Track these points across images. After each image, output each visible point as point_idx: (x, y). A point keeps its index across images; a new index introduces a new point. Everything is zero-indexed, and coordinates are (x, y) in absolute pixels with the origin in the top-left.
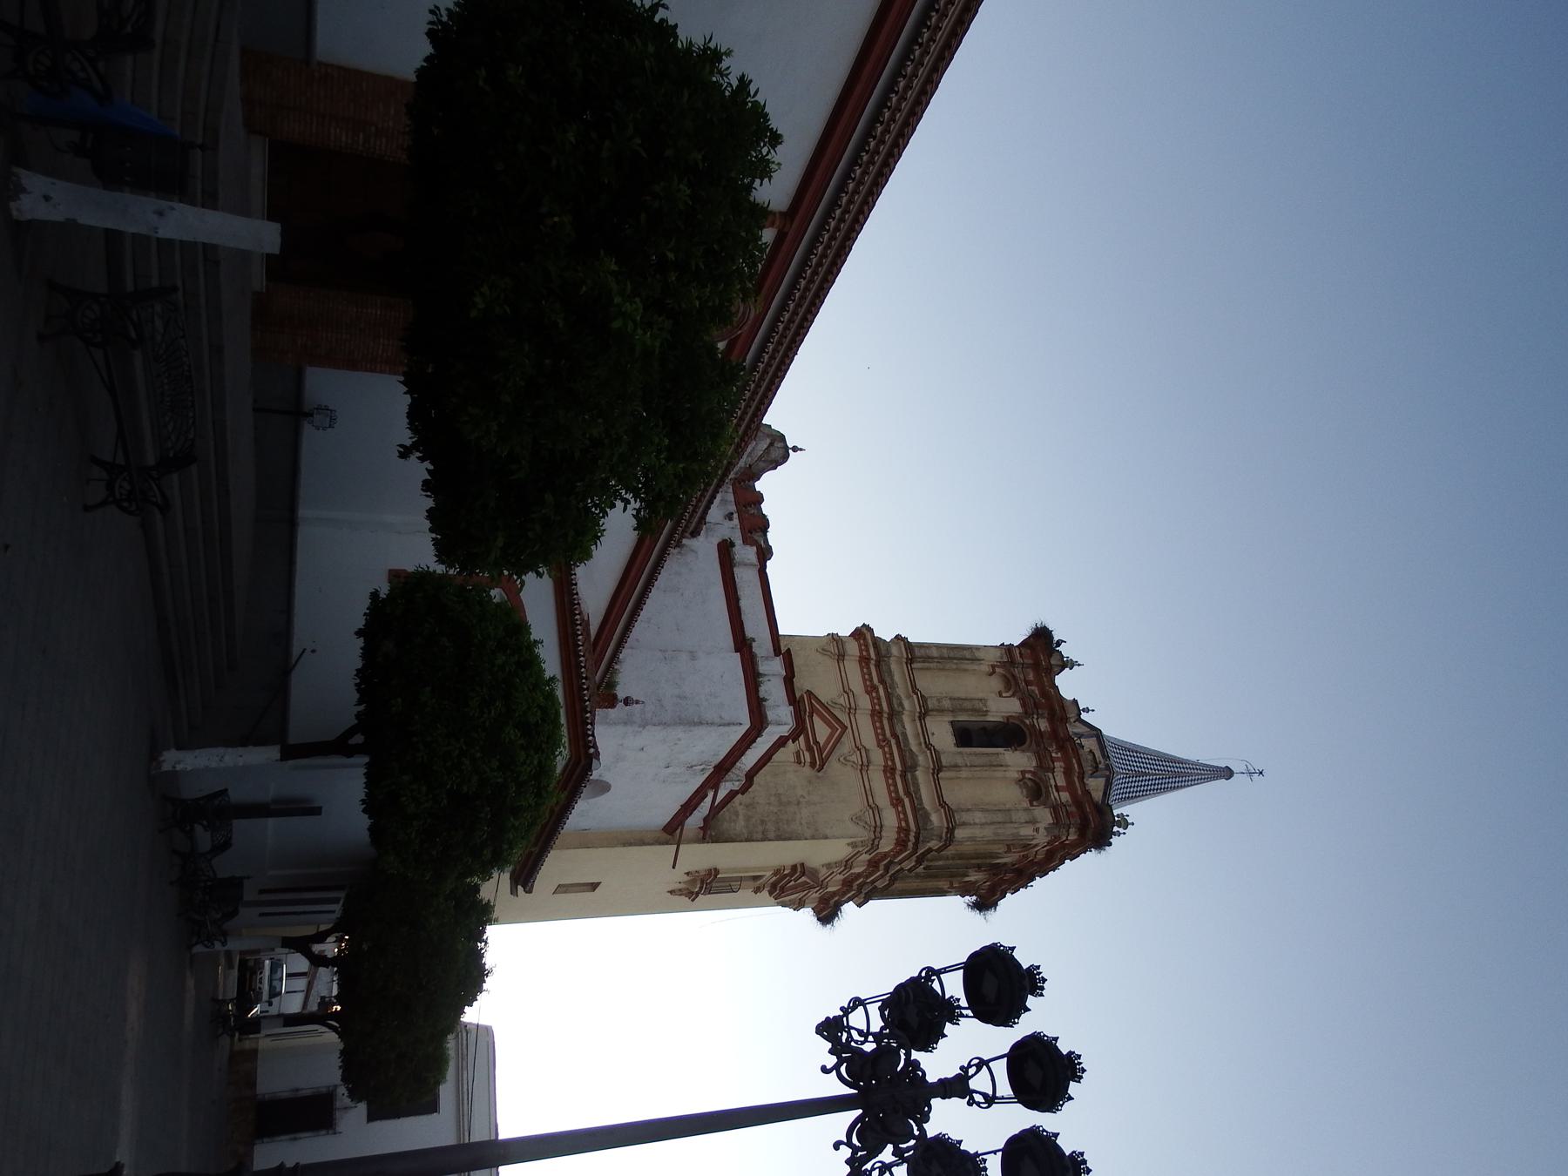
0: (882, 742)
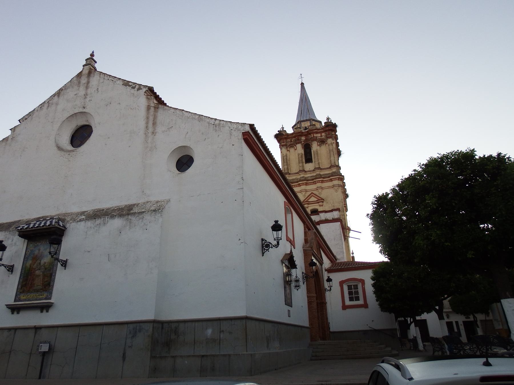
0: (315, 183)
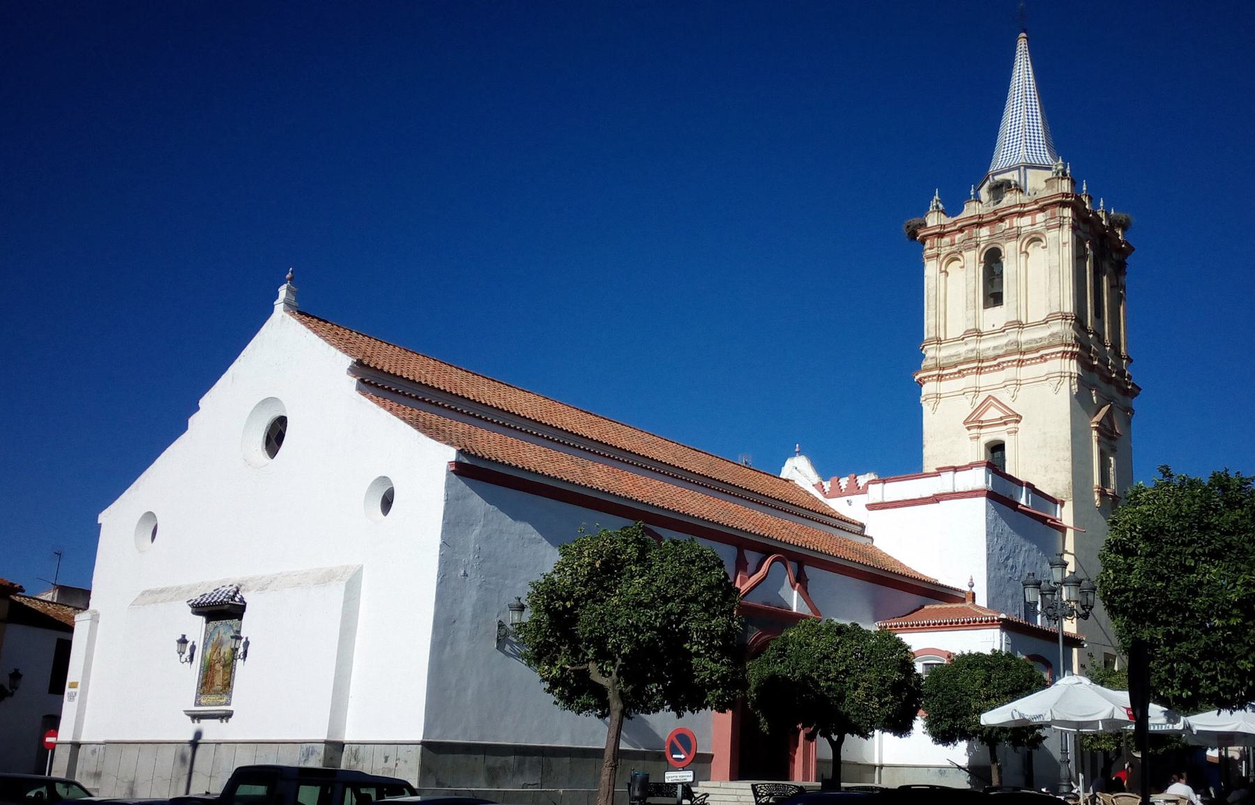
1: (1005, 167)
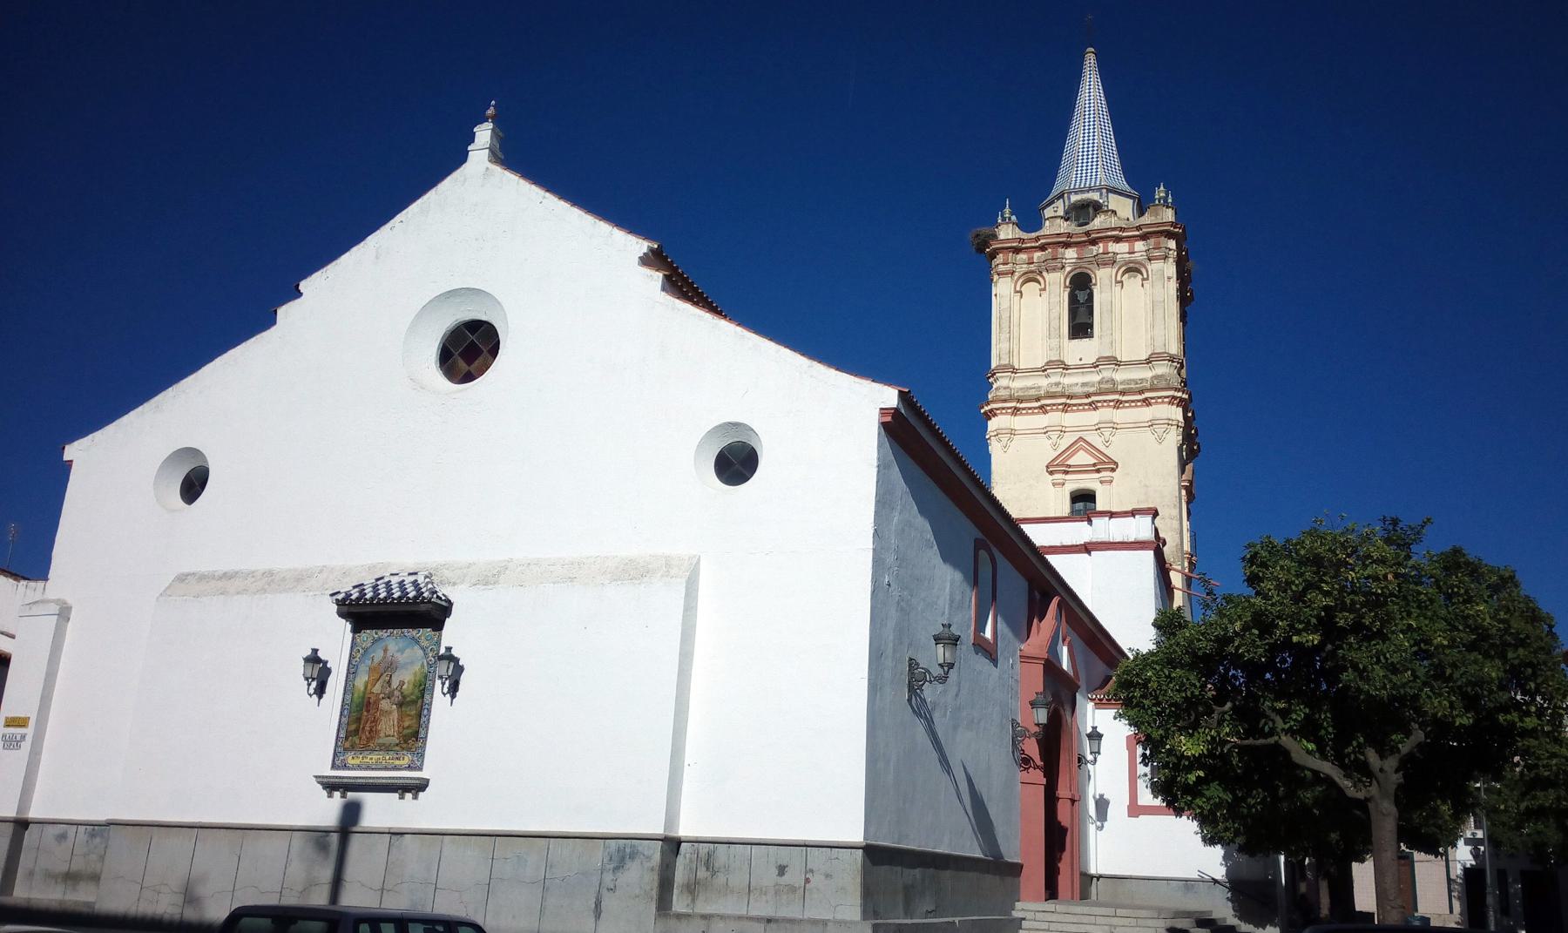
0: (1093, 406)
1: (1085, 187)
